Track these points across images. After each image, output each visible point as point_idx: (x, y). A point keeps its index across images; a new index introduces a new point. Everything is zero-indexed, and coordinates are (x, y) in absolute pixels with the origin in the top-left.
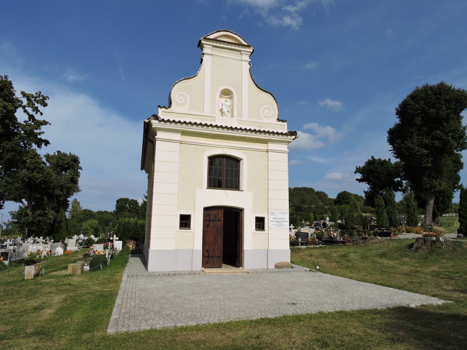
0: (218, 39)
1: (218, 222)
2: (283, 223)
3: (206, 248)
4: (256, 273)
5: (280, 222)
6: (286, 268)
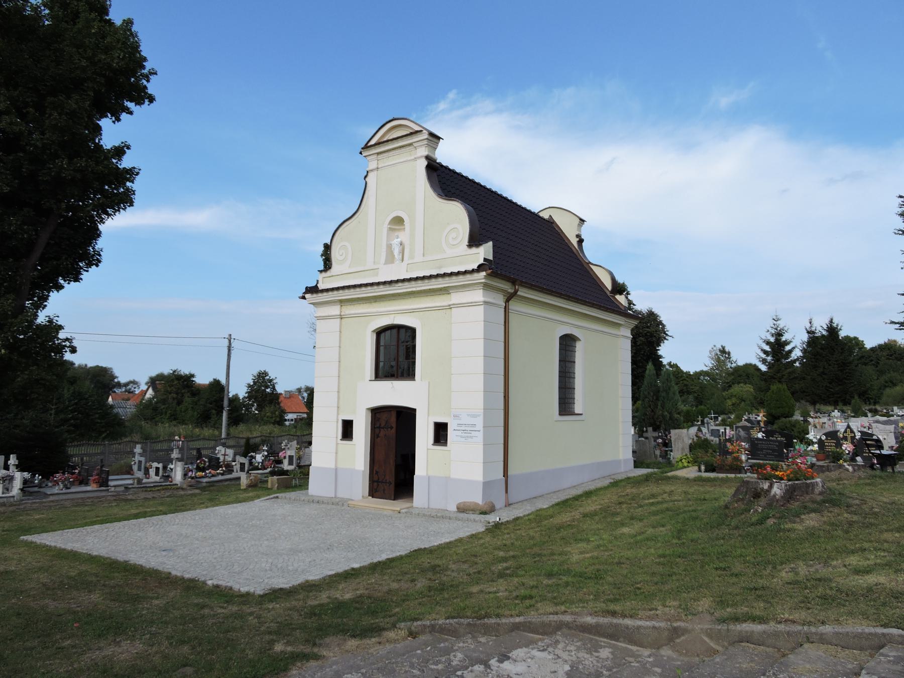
0: (385, 139)
1: (389, 429)
2: (473, 433)
3: (376, 468)
4: (319, 501)
5: (469, 432)
6: (471, 512)
